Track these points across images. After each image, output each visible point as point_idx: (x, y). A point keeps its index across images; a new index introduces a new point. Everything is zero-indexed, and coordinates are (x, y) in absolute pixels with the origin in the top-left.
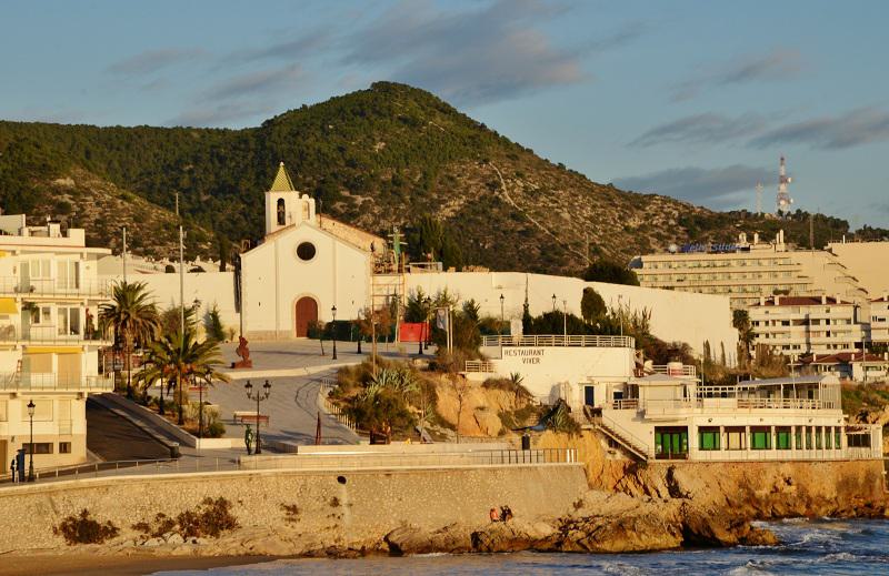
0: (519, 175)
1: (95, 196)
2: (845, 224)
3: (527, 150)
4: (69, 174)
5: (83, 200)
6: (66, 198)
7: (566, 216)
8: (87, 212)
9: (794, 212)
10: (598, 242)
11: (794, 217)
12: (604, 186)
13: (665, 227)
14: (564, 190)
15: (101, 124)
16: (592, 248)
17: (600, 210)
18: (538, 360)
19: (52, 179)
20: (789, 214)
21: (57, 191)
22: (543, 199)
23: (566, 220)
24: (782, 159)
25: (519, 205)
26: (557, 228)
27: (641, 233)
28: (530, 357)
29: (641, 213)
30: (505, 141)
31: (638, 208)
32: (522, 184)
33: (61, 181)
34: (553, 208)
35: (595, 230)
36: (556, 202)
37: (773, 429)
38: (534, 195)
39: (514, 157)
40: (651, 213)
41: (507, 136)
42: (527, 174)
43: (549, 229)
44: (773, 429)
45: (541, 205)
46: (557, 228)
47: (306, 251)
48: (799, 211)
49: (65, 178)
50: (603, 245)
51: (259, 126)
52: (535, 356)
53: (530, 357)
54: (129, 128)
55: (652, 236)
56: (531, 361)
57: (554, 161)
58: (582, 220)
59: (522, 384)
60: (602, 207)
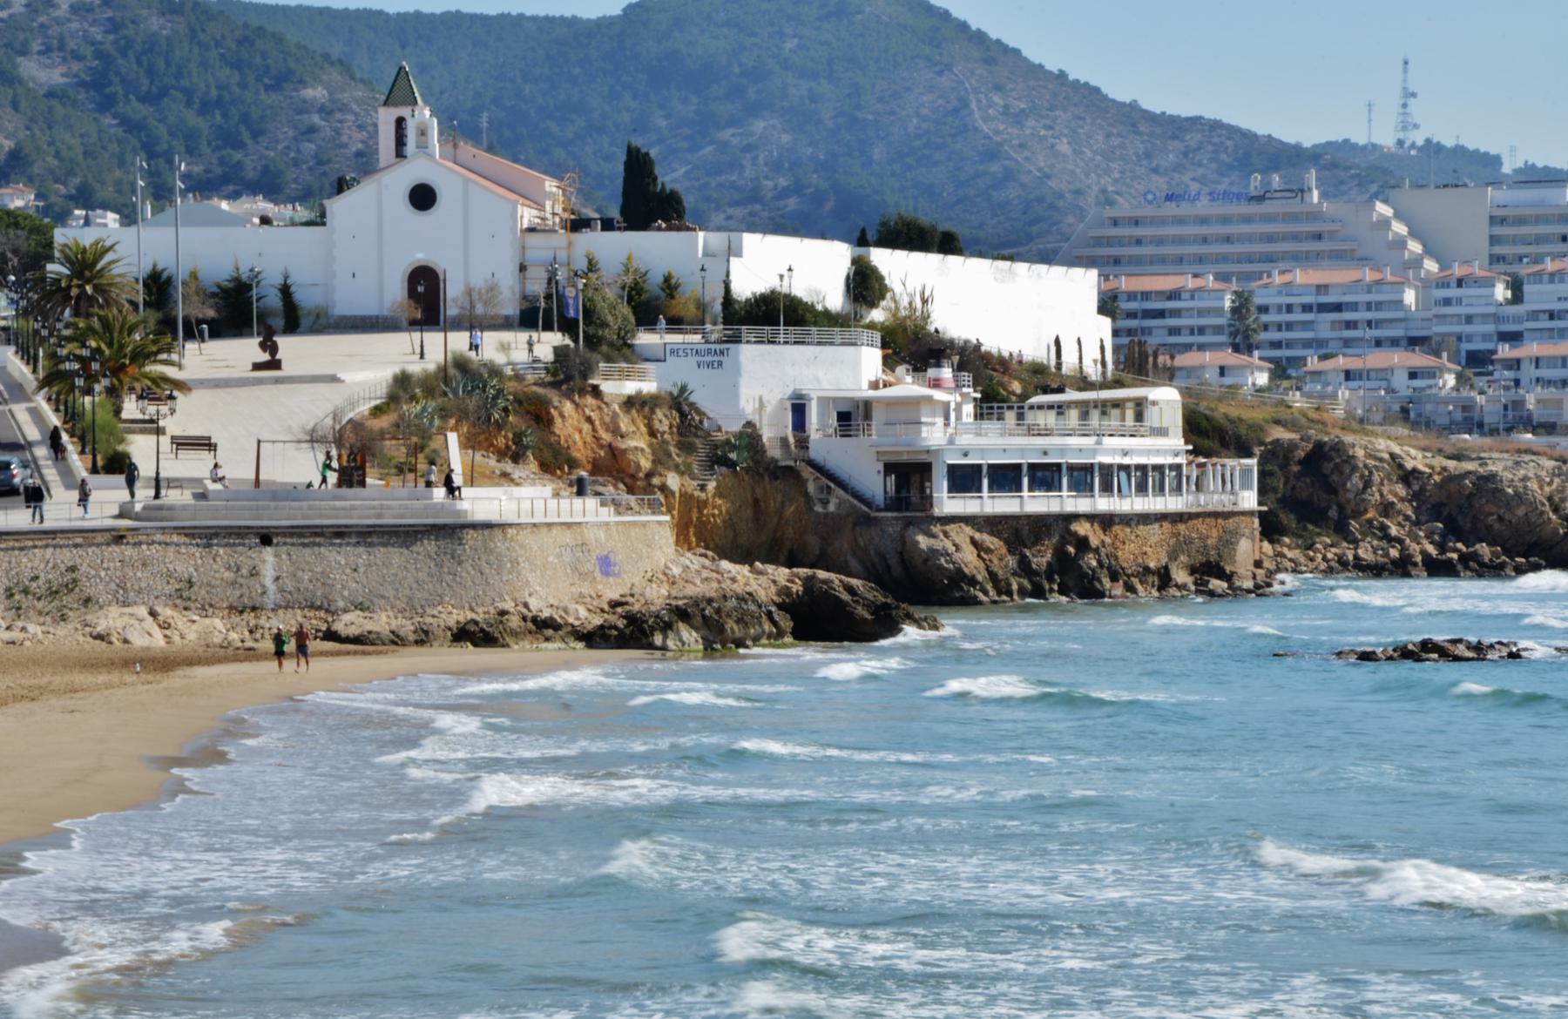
0: (999, 88)
1: (356, 115)
2: (1495, 161)
3: (273, 35)
4: (321, 82)
5: (340, 121)
6: (316, 119)
7: (1064, 147)
8: (345, 139)
9: (1420, 143)
10: (1110, 189)
11: (1420, 149)
12: (1124, 104)
13: (1213, 166)
14: (1064, 109)
15: (391, 9)
16: (1102, 198)
17: (1116, 141)
18: (720, 364)
19: (296, 90)
20: (1413, 146)
21: (303, 108)
22: (1031, 123)
23: (1064, 155)
24: (1406, 63)
25: (997, 132)
26: (1052, 166)
27: (1176, 175)
28: (709, 358)
29: (1177, 144)
30: (980, 37)
31: (1174, 137)
32: (1001, 102)
33: (309, 93)
34: (1045, 137)
35: (1108, 171)
36: (1051, 128)
37: (1025, 469)
38: (1018, 118)
39: (989, 62)
40: (1193, 144)
41: (984, 29)
42: (1010, 86)
43: (1040, 170)
44: (1025, 469)
45: (1028, 132)
46: (1052, 166)
47: (423, 197)
48: (1428, 141)
49: (314, 88)
50: (1117, 193)
51: (974, 28)
52: (716, 358)
53: (709, 358)
54: (433, 15)
55: (1193, 179)
56: (710, 365)
57: (1052, 66)
58: (1089, 154)
59: (692, 398)
60: (1119, 135)
